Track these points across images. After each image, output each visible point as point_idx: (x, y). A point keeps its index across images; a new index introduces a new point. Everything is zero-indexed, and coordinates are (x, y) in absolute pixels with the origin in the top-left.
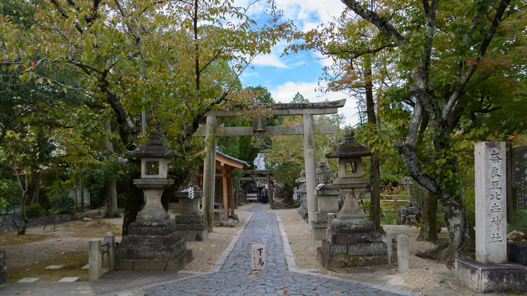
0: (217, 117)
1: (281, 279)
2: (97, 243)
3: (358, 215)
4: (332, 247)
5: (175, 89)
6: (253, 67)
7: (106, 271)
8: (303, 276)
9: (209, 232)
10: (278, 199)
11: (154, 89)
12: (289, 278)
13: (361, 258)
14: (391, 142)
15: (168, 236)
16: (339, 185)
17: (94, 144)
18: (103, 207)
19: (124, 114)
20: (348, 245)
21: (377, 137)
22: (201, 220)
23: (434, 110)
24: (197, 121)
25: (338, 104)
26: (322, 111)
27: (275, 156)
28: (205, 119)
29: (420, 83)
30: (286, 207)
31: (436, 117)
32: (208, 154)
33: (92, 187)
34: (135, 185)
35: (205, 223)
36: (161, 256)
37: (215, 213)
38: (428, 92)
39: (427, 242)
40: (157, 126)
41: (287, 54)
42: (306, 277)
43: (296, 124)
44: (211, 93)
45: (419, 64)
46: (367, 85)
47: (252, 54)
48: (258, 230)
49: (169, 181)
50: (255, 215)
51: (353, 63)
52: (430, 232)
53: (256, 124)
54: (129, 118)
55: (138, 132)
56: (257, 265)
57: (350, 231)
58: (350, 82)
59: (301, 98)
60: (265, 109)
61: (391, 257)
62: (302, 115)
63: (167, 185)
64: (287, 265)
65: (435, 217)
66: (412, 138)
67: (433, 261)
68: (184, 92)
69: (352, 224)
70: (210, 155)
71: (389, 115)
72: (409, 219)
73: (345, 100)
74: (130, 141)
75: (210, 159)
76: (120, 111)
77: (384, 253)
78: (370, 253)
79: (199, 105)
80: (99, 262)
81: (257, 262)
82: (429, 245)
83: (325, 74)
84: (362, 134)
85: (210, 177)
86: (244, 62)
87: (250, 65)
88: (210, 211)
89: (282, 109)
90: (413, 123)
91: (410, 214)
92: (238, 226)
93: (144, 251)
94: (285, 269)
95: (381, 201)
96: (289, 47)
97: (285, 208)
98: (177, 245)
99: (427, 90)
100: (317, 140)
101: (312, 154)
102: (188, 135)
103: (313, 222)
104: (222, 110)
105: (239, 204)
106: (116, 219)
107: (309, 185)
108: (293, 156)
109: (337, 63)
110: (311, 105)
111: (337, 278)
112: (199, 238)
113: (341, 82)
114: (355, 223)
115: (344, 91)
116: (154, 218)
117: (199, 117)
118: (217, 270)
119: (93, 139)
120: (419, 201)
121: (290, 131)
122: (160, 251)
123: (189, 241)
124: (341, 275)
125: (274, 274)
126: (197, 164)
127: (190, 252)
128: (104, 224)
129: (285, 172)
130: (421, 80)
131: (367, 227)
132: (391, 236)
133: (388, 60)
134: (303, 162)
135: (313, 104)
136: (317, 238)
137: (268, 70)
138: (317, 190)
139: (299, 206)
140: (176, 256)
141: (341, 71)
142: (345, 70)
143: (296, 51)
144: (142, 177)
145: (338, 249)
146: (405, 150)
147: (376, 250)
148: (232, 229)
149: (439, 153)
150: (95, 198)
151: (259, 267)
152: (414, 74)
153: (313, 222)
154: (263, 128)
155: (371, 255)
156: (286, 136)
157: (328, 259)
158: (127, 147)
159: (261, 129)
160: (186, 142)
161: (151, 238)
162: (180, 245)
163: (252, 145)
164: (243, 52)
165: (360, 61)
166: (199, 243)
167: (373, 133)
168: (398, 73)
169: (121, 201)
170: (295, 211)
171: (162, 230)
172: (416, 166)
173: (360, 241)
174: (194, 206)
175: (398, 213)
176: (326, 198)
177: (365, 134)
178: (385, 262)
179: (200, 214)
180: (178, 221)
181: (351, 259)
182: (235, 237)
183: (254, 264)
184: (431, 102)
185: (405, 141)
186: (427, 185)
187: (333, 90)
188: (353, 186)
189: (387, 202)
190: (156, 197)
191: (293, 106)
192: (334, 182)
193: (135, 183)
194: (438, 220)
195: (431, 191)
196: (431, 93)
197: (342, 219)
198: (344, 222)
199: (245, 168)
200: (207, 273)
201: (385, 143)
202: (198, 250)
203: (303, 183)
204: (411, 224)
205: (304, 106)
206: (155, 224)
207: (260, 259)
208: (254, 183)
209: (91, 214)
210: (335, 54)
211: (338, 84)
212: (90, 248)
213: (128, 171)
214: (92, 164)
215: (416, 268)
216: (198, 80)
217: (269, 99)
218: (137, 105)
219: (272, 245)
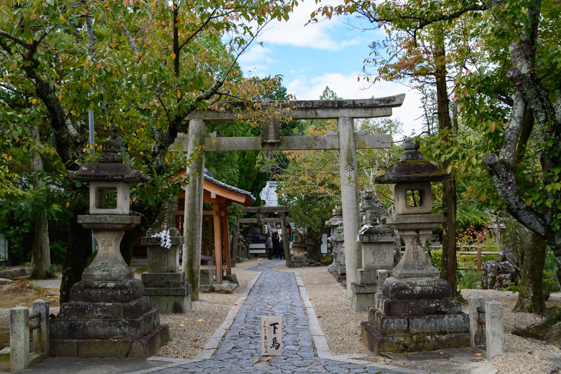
0: (204, 121)
1: (306, 369)
2: (22, 313)
3: (424, 271)
4: (385, 321)
5: (141, 77)
6: (261, 43)
7: (36, 356)
8: (341, 365)
9: (193, 300)
10: (298, 252)
11: (110, 74)
12: (319, 367)
13: (429, 337)
14: (477, 158)
15: (132, 304)
16: (396, 224)
17: (13, 164)
18: (28, 263)
19: (63, 114)
20: (409, 318)
21: (455, 149)
22: (181, 281)
23: (543, 107)
24: (175, 125)
25: (393, 101)
26: (368, 112)
27: (294, 184)
28: (187, 125)
29: (521, 66)
30: (311, 265)
31: (547, 118)
32: (191, 178)
33: (11, 232)
34: (80, 224)
35: (186, 286)
36: (122, 334)
37: (202, 271)
38: (534, 80)
39: (528, 314)
40: (112, 133)
41: (316, 20)
42: (345, 366)
43: (327, 133)
44: (198, 82)
45: (521, 36)
46: (437, 71)
47: (260, 21)
48: (269, 298)
49: (133, 218)
50: (263, 276)
51: (417, 37)
52: (533, 298)
53: (267, 132)
54: (69, 121)
55: (84, 141)
56: (269, 348)
57: (413, 297)
58: (411, 67)
59: (333, 95)
60: (280, 109)
61: (475, 336)
62: (337, 118)
63: (130, 224)
64: (315, 348)
65: (541, 275)
66: (509, 150)
67: (539, 341)
68: (155, 80)
69: (415, 285)
70: (194, 181)
71: (475, 115)
72: (501, 281)
73: (404, 95)
74: (71, 156)
75: (194, 187)
76: (56, 109)
77: (464, 330)
78: (443, 330)
79: (179, 100)
80: (25, 343)
81: (270, 343)
82: (532, 318)
83: (373, 54)
84: (433, 145)
85: (195, 215)
86: (248, 33)
87: (258, 39)
88: (195, 268)
89: (307, 109)
90: (510, 127)
91: (501, 273)
92: (238, 292)
93: (95, 326)
94: (313, 354)
95: (458, 253)
96: (319, 10)
97: (308, 266)
98: (145, 318)
99: (533, 76)
100: (360, 159)
101: (353, 179)
102: (161, 147)
103: (354, 284)
104: (214, 110)
105: (237, 259)
106: (50, 281)
107: (348, 230)
108: (321, 184)
109: (392, 37)
110: (351, 103)
111: (392, 367)
112: (178, 309)
113: (399, 67)
114: (421, 283)
115: (401, 80)
116: (110, 275)
117: (179, 119)
118: (207, 355)
119: (13, 156)
120: (517, 251)
121: (318, 143)
122: (120, 327)
123: (163, 313)
124: (399, 362)
125: (296, 362)
126: (174, 194)
127: (165, 330)
128: (30, 287)
129: (309, 210)
130: (524, 61)
131: (438, 290)
132: (476, 303)
133: (472, 31)
134: (339, 193)
135: (354, 101)
136: (361, 309)
137: (285, 51)
138: (361, 235)
139: (331, 263)
140: (145, 335)
141: (399, 48)
142: (404, 48)
143: (330, 16)
144: (91, 212)
145: (394, 324)
146: (499, 170)
147: (453, 324)
148: (229, 296)
149: (550, 174)
150: (16, 249)
151: (272, 351)
152: (513, 52)
153: (354, 284)
154: (277, 138)
155: (445, 333)
156: (312, 152)
157: (379, 338)
158: (66, 166)
159: (273, 141)
160: (158, 158)
161: (105, 306)
162: (150, 318)
163: (258, 169)
164: (248, 18)
165: (427, 34)
166: (178, 317)
167: (449, 144)
168: (486, 52)
169: (56, 253)
170: (324, 269)
171: (123, 293)
172: (516, 194)
173: (428, 312)
174: (171, 259)
175: (483, 272)
176: (374, 248)
177: (436, 144)
178: (466, 342)
179: (180, 272)
180: (146, 281)
181: (414, 339)
182: (234, 307)
183: (264, 346)
184: (538, 95)
185: (498, 155)
186: (531, 223)
187: (385, 78)
188: (417, 227)
189: (466, 255)
190: (113, 243)
191: (324, 105)
192: (389, 221)
193: (80, 222)
194: (545, 280)
195: (537, 233)
196: (538, 81)
197: (400, 277)
198: (404, 282)
199: (249, 202)
200: (192, 361)
201: (468, 158)
202: (177, 326)
203: (337, 226)
204: (502, 286)
205: (340, 105)
206: (111, 285)
207: (275, 340)
208: (261, 227)
209: (9, 272)
210: (390, 21)
211: (393, 70)
212: (12, 321)
213: (68, 204)
214: (12, 194)
215: (513, 351)
216: (177, 62)
217: (283, 96)
218: (81, 100)
219: (291, 320)
